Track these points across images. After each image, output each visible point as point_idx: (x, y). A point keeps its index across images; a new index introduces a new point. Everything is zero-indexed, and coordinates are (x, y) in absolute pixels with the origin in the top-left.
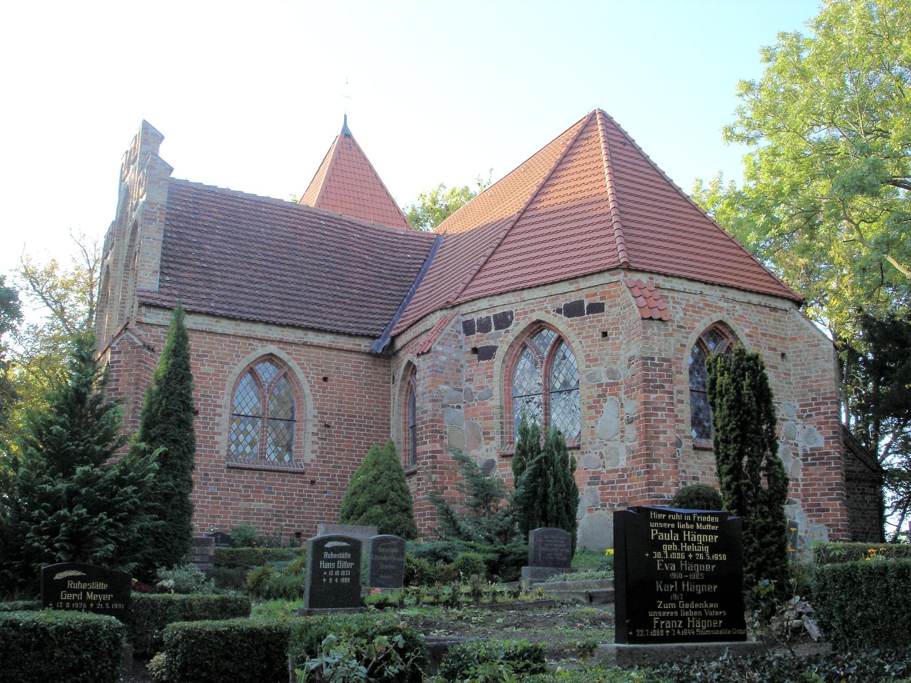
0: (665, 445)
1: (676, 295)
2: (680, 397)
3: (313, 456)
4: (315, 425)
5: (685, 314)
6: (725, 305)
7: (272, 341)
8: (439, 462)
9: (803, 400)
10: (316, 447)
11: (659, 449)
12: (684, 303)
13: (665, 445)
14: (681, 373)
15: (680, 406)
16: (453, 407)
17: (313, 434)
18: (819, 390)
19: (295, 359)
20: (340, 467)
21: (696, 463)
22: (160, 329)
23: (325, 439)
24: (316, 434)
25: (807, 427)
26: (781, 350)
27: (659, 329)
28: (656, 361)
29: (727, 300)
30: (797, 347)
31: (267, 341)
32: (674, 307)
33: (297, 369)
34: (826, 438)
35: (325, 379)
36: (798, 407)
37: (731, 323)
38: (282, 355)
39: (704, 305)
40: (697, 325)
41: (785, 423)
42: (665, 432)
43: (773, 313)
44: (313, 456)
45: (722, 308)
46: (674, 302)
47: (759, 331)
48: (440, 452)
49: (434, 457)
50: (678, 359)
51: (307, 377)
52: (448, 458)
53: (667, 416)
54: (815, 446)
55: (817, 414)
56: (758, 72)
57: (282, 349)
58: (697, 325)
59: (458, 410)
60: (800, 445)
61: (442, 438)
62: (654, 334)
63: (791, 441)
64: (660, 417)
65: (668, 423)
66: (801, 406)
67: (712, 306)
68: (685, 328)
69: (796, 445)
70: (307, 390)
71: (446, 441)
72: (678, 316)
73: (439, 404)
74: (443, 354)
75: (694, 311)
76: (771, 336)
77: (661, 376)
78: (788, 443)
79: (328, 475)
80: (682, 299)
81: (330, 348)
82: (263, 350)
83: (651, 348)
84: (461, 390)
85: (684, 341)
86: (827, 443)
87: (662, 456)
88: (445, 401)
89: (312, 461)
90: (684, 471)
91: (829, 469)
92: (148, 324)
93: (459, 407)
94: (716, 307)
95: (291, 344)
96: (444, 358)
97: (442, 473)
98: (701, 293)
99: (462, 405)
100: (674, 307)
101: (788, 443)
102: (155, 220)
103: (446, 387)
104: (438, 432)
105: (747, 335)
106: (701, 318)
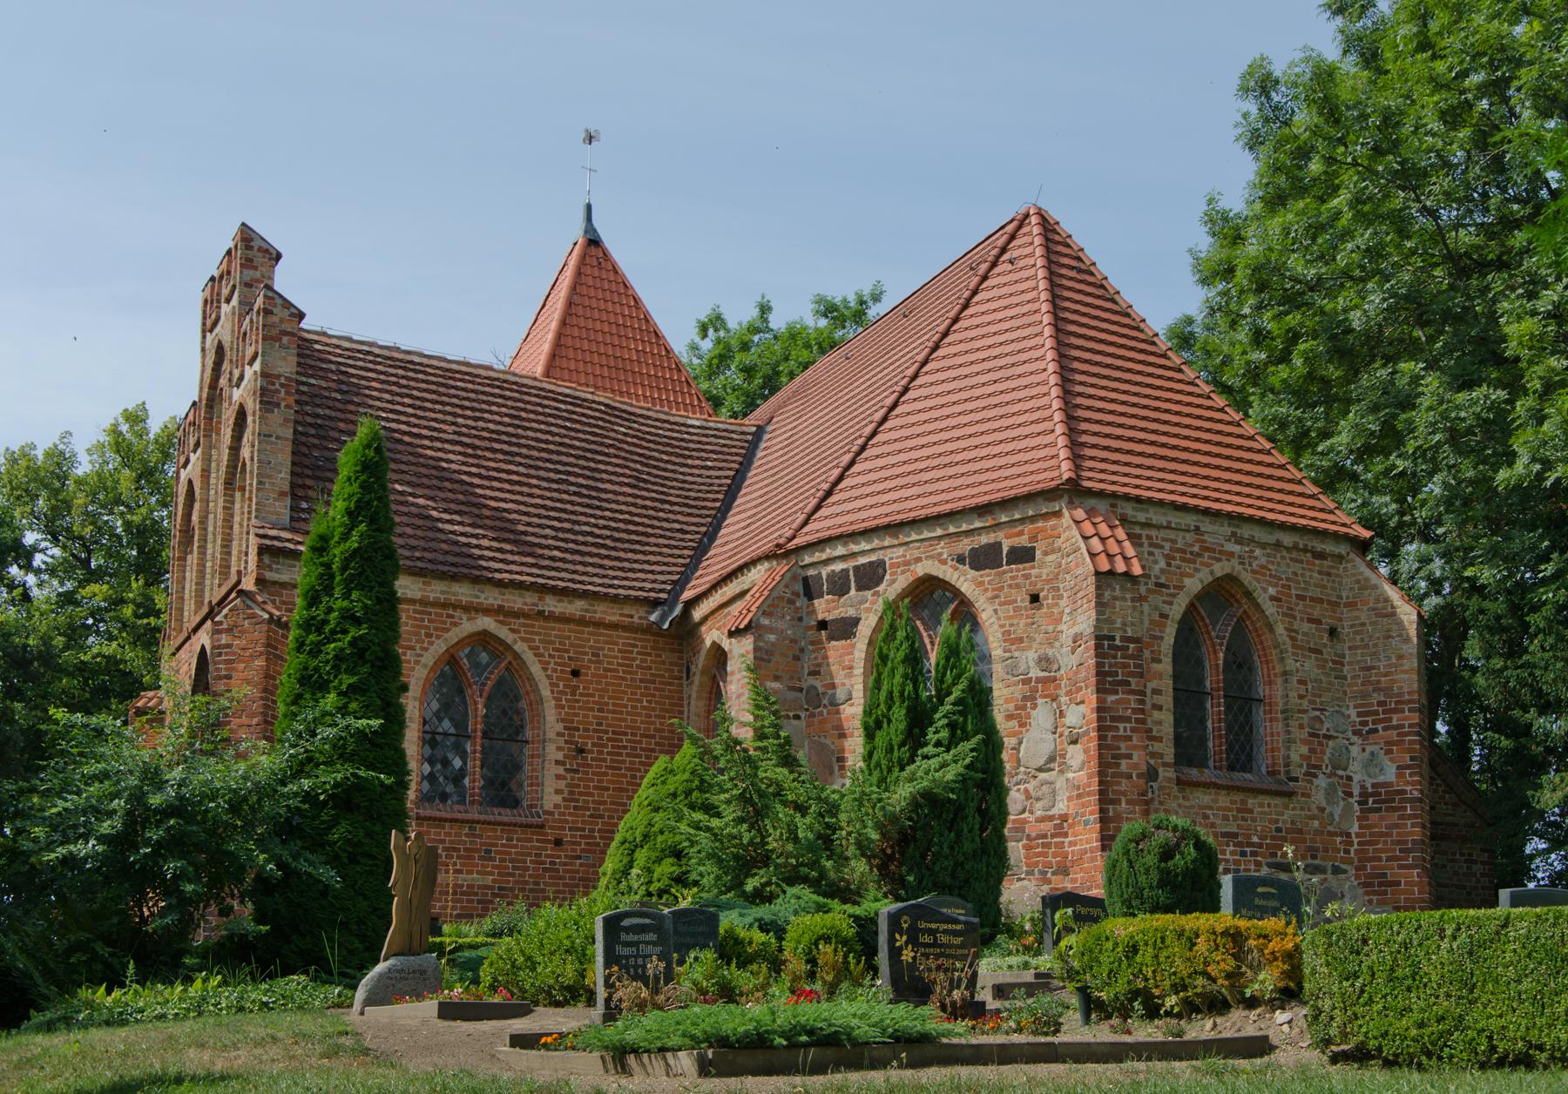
1: (1154, 533)
3: (558, 799)
4: (559, 749)
5: (1169, 565)
6: (1236, 548)
7: (487, 611)
10: (562, 784)
11: (1119, 784)
12: (1167, 545)
13: (1129, 776)
14: (1160, 661)
15: (1156, 715)
17: (557, 762)
19: (523, 639)
20: (601, 817)
21: (1180, 806)
23: (576, 771)
26: (1328, 621)
27: (1123, 588)
28: (1117, 642)
30: (1357, 618)
31: (477, 610)
33: (529, 657)
34: (1399, 768)
35: (575, 673)
36: (1354, 717)
37: (1246, 578)
38: (504, 633)
40: (1187, 581)
41: (1331, 743)
42: (1129, 756)
43: (1317, 562)
44: (558, 799)
45: (1232, 554)
46: (1151, 545)
47: (1294, 592)
50: (1155, 638)
51: (545, 669)
54: (1381, 779)
55: (1385, 729)
58: (1187, 581)
59: (795, 722)
60: (1356, 778)
62: (1115, 598)
63: (1340, 772)
64: (1121, 732)
66: (1359, 714)
67: (1214, 551)
69: (1350, 778)
74: (771, 630)
75: (1183, 560)
76: (1312, 599)
77: (1125, 666)
78: (1335, 775)
79: (584, 830)
80: (1163, 539)
81: (582, 622)
83: (1110, 621)
84: (801, 690)
86: (1400, 775)
87: (1124, 793)
89: (556, 806)
91: (1402, 817)
92: (275, 583)
93: (797, 717)
98: (1197, 528)
99: (803, 715)
101: (1335, 775)
102: (278, 405)
103: (775, 685)
105: (1272, 598)
106: (1196, 570)
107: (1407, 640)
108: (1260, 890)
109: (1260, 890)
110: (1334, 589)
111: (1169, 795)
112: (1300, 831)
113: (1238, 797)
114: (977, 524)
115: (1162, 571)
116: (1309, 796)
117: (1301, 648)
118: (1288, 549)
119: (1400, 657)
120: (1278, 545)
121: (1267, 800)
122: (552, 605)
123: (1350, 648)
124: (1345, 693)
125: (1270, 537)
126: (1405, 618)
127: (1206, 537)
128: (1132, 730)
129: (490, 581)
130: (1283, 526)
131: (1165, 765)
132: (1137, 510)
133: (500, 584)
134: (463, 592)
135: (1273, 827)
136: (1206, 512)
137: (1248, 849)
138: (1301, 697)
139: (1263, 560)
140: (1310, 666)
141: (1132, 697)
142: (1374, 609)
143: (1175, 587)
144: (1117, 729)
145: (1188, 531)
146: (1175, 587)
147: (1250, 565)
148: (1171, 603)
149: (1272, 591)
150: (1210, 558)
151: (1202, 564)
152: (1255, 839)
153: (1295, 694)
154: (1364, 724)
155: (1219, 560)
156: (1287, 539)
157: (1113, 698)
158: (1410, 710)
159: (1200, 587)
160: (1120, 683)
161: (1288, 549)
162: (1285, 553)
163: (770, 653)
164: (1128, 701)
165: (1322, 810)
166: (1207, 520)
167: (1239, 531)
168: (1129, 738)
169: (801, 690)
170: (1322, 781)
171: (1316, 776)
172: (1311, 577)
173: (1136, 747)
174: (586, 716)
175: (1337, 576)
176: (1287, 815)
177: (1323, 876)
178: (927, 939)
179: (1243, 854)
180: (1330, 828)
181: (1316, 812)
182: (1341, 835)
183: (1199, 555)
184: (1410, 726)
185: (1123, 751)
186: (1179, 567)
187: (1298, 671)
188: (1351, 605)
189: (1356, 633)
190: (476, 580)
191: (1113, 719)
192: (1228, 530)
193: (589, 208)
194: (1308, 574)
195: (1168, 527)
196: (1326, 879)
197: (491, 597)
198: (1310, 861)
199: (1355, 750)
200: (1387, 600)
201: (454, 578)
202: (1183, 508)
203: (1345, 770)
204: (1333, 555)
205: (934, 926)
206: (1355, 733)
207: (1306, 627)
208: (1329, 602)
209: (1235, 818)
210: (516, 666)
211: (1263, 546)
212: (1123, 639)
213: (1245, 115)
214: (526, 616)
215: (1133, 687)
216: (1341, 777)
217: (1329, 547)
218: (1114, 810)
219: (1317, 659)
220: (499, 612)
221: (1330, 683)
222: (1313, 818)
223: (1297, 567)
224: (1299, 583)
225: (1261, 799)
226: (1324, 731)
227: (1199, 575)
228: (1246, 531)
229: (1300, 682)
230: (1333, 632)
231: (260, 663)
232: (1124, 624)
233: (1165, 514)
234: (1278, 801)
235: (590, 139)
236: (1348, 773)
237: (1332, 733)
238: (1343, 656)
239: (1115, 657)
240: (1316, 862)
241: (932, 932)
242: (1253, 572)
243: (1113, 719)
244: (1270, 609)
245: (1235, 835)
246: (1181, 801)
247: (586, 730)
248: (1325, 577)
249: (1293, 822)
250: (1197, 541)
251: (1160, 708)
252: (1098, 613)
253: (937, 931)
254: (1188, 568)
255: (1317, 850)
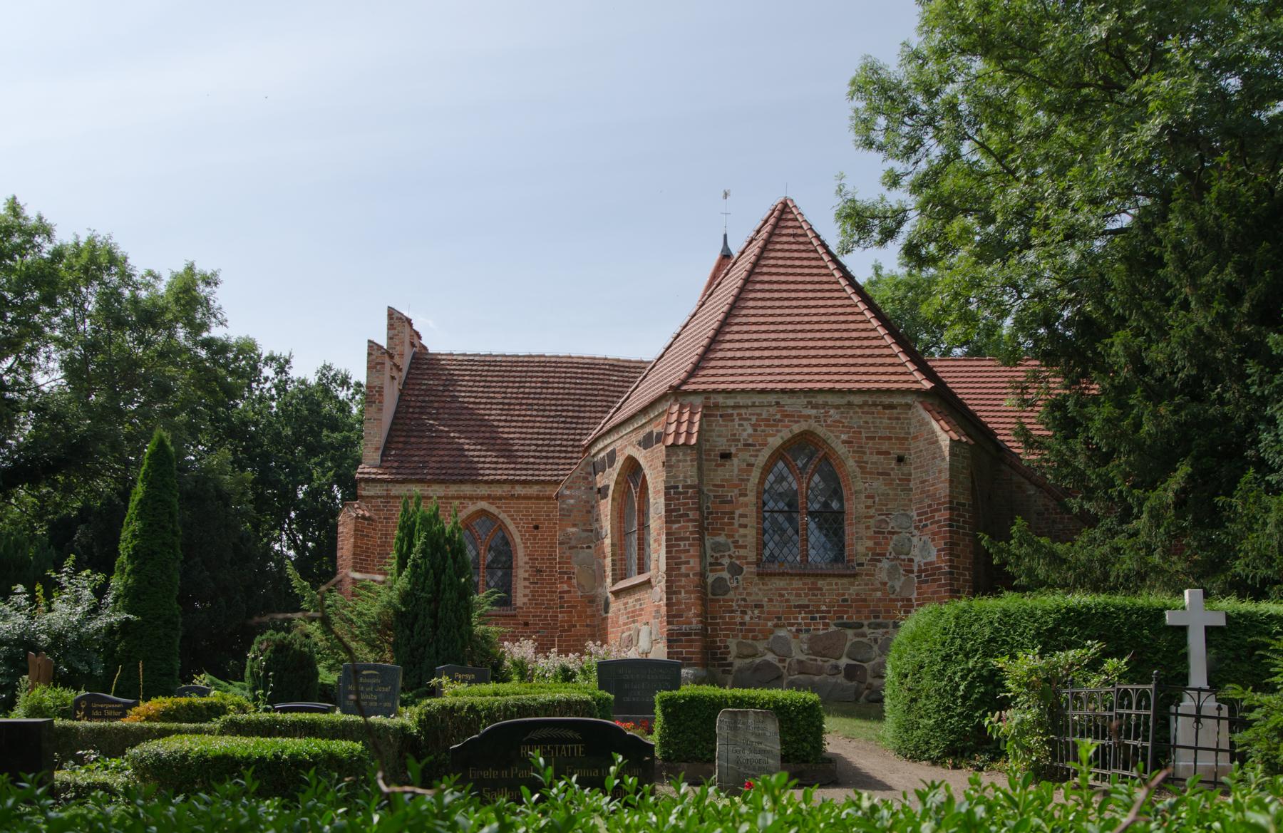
0: (687, 575)
1: (743, 411)
2: (743, 521)
3: (526, 600)
4: (526, 571)
5: (755, 430)
6: (813, 412)
7: (482, 498)
8: (565, 602)
9: (920, 508)
10: (527, 591)
11: (680, 581)
12: (754, 418)
13: (687, 575)
14: (746, 495)
15: (742, 531)
16: (582, 548)
17: (525, 579)
18: (935, 495)
19: (504, 512)
20: (552, 608)
21: (760, 589)
22: (379, 500)
23: (537, 583)
24: (528, 579)
25: (923, 538)
26: (896, 452)
27: (685, 454)
28: (680, 490)
29: (816, 407)
30: (918, 447)
31: (477, 499)
32: (740, 425)
33: (508, 521)
34: (938, 551)
35: (536, 527)
36: (916, 518)
37: (821, 431)
38: (493, 509)
39: (782, 416)
40: (770, 440)
41: (895, 537)
42: (688, 563)
43: (887, 411)
44: (526, 600)
45: (809, 416)
46: (740, 420)
47: (864, 435)
48: (569, 592)
49: (561, 598)
50: (743, 480)
51: (517, 527)
52: (577, 597)
53: (690, 545)
54: (929, 559)
55: (931, 524)
56: (83, 240)
57: (492, 504)
58: (770, 440)
59: (588, 551)
60: (916, 560)
61: (570, 578)
62: (679, 461)
63: (903, 557)
64: (682, 548)
65: (692, 552)
66: (919, 515)
67: (793, 416)
68: (754, 445)
69: (911, 560)
70: (518, 540)
71: (574, 581)
72: (745, 434)
73: (566, 546)
74: (571, 497)
75: (766, 426)
76: (880, 438)
77: (685, 504)
78: (898, 559)
79: (540, 616)
80: (750, 414)
81: (538, 498)
82: (472, 508)
83: (675, 476)
84: (592, 531)
85: (752, 460)
86: (939, 556)
87: (684, 587)
88: (573, 543)
89: (524, 604)
90: (744, 600)
91: (939, 586)
92: (368, 497)
93: (589, 547)
94: (799, 417)
95: (500, 498)
96: (572, 501)
97: (571, 612)
98: (778, 403)
99: (593, 545)
100: (740, 425)
101: (898, 559)
102: (375, 402)
103: (574, 530)
104: (565, 573)
105: (844, 442)
106: (777, 431)
107: (944, 459)
108: (364, 673)
109: (364, 673)
110: (902, 428)
111: (751, 583)
112: (865, 600)
113: (809, 581)
114: (644, 421)
115: (750, 435)
116: (873, 575)
117: (870, 473)
118: (860, 406)
119: (940, 472)
120: (850, 405)
121: (834, 581)
122: (519, 490)
123: (915, 469)
124: (911, 500)
125: (843, 401)
126: (942, 443)
127: (786, 408)
128: (690, 545)
129: (481, 481)
130: (850, 391)
131: (748, 563)
132: (726, 398)
133: (486, 482)
134: (467, 489)
135: (840, 599)
136: (783, 391)
137: (818, 615)
138: (868, 507)
139: (837, 417)
140: (878, 485)
141: (690, 524)
142: (926, 439)
143: (760, 445)
144: (679, 545)
145: (771, 406)
146: (760, 445)
147: (825, 421)
148: (757, 456)
149: (843, 437)
150: (789, 421)
151: (782, 426)
152: (824, 608)
153: (863, 506)
154: (920, 521)
155: (797, 422)
156: (857, 400)
157: (676, 526)
158: (945, 509)
159: (781, 442)
160: (682, 516)
161: (860, 406)
162: (857, 409)
163: (570, 511)
164: (688, 527)
165: (885, 584)
166: (786, 396)
167: (814, 400)
168: (688, 551)
169: (592, 531)
170: (885, 564)
171: (880, 561)
172: (881, 423)
173: (692, 556)
174: (542, 551)
175: (906, 419)
176: (853, 590)
177: (885, 630)
178: (97, 713)
179: (813, 618)
180: (892, 596)
181: (879, 586)
182: (902, 600)
183: (780, 421)
184: (945, 520)
185: (683, 559)
186: (763, 431)
187: (866, 489)
188: (915, 438)
189: (918, 457)
190: (474, 482)
191: (676, 539)
192: (805, 401)
193: (725, 236)
194: (878, 421)
195: (754, 405)
196: (887, 632)
197: (483, 490)
198: (873, 620)
199: (915, 540)
200: (933, 432)
201: (461, 482)
202: (763, 391)
203: (907, 554)
204: (901, 405)
205: (102, 706)
206: (917, 528)
207: (875, 458)
208: (897, 438)
209: (806, 595)
210: (502, 527)
211: (837, 407)
212: (684, 487)
213: (856, 110)
214: (506, 498)
215: (691, 517)
216: (904, 560)
217: (896, 400)
218: (677, 598)
219: (884, 479)
220: (488, 498)
221: (896, 495)
222: (877, 590)
223: (869, 418)
224: (869, 428)
225: (829, 580)
226: (890, 529)
227: (779, 434)
228: (820, 399)
229: (868, 497)
230: (900, 459)
231: (352, 540)
232: (685, 477)
233: (750, 398)
234: (845, 581)
235: (726, 195)
236: (910, 556)
237: (896, 529)
238: (910, 474)
239: (678, 499)
240: (878, 621)
241: (100, 709)
242: (827, 426)
243: (676, 539)
244: (842, 450)
245: (808, 606)
246: (761, 586)
247: (543, 559)
248: (895, 422)
249: (857, 595)
250: (778, 412)
251: (745, 526)
252: (668, 472)
253: (104, 708)
254: (770, 431)
255: (880, 612)
